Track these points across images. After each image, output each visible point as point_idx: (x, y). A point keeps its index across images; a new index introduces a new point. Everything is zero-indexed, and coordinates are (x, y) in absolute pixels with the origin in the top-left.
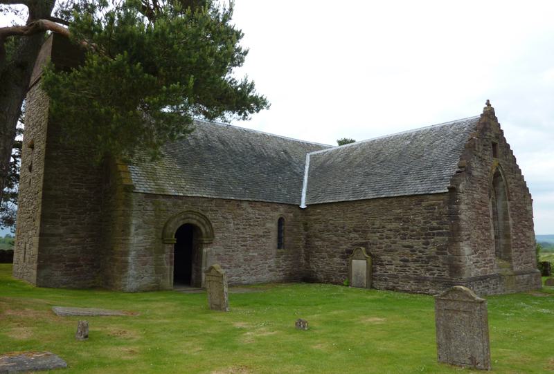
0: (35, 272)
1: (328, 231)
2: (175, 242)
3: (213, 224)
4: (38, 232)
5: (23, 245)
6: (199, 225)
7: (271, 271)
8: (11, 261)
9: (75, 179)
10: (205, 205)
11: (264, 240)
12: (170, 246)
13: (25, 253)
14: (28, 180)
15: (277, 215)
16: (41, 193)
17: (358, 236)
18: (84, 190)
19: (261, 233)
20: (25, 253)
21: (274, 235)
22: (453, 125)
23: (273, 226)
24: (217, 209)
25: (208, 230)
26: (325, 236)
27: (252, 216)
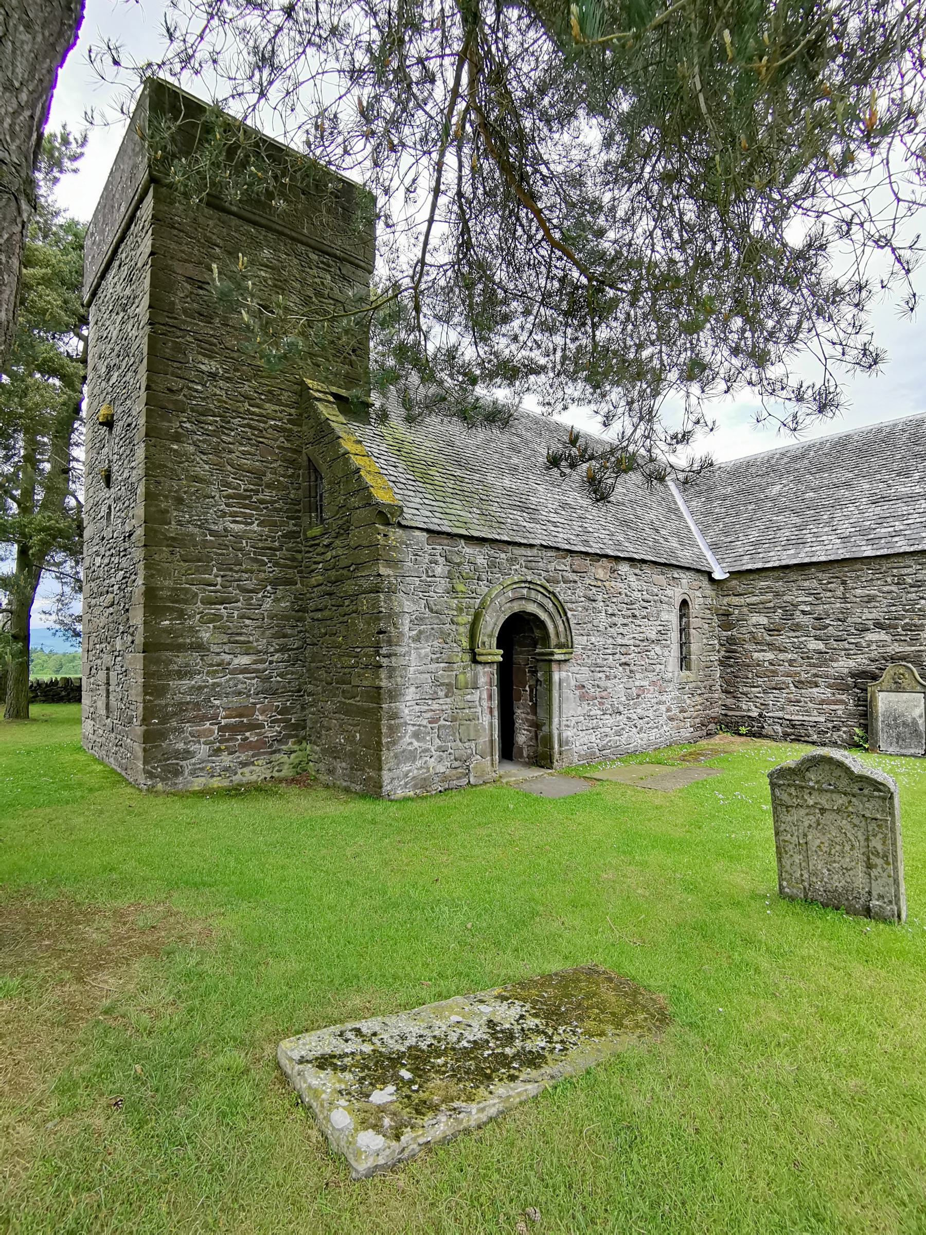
0: (138, 749)
1: (796, 628)
2: (501, 659)
3: (569, 614)
4: (139, 639)
5: (102, 675)
6: (543, 616)
7: (671, 719)
8: (79, 700)
9: (228, 497)
10: (551, 567)
11: (658, 649)
12: (487, 669)
13: (108, 697)
14: (104, 509)
15: (677, 594)
16: (140, 532)
17: (888, 638)
18: (255, 527)
19: (653, 636)
20: (108, 697)
21: (674, 636)
22: (803, 456)
23: (671, 617)
24: (574, 577)
25: (561, 628)
26: (781, 639)
27: (637, 594)
